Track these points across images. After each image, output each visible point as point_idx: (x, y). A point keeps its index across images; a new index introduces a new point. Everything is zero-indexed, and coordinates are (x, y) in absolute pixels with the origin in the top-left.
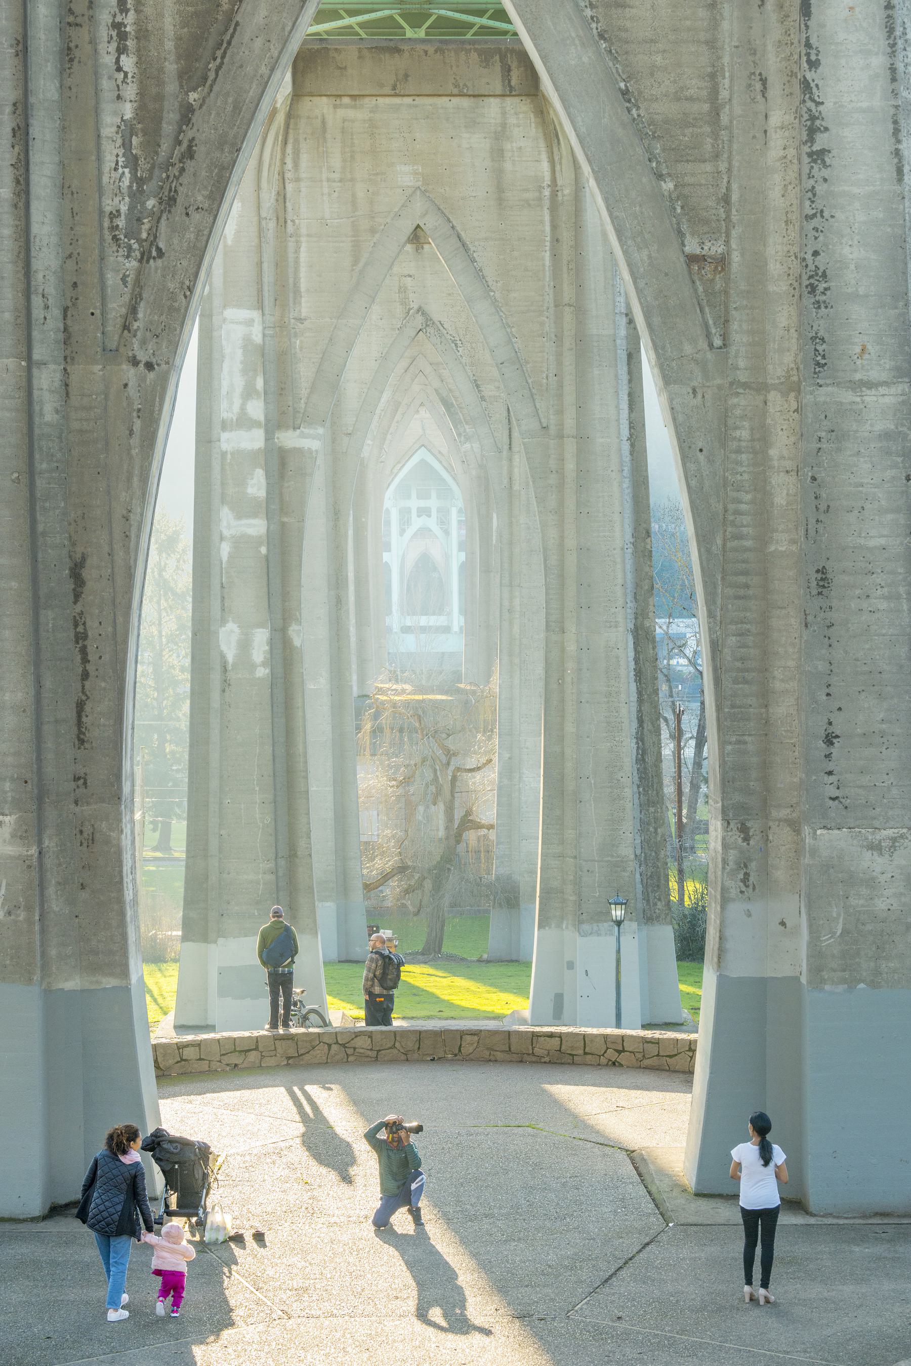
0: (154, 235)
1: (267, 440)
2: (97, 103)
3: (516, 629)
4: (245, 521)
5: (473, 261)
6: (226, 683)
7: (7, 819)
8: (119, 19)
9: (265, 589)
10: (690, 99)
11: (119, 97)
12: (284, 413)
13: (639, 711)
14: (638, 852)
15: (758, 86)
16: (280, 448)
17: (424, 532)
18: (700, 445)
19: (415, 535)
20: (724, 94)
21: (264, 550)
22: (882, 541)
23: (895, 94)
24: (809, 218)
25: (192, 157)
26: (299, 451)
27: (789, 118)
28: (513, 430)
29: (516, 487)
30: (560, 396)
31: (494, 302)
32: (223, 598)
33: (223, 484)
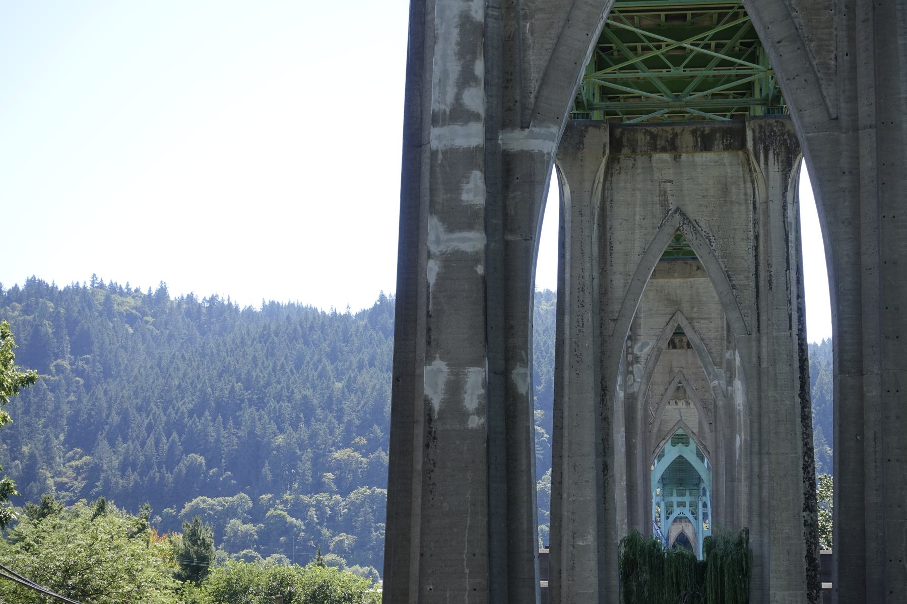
1: (487, 139)
3: (765, 493)
4: (457, 235)
9: (482, 318)
12: (510, 109)
16: (504, 151)
19: (675, 520)
21: (480, 269)
26: (529, 156)
28: (761, 315)
29: (764, 365)
30: (853, 79)
32: (429, 330)
33: (432, 190)
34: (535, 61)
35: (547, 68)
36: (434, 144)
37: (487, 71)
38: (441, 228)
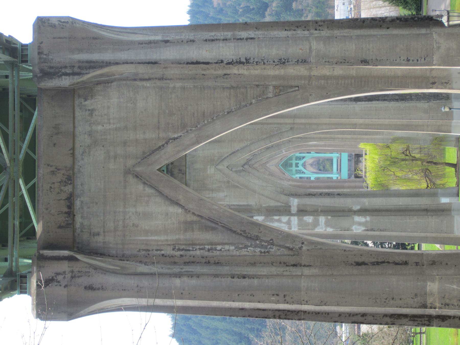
0: (266, 242)
2: (230, 256)
4: (320, 223)
5: (238, 150)
6: (372, 230)
7: (428, 284)
8: (207, 250)
10: (230, 95)
11: (228, 250)
13: (381, 100)
14: (426, 101)
15: (226, 76)
17: (304, 165)
18: (325, 94)
19: (305, 168)
20: (229, 86)
21: (329, 217)
22: (354, 45)
23: (230, 39)
24: (264, 64)
25: (245, 231)
27: (236, 68)
30: (281, 124)
31: (251, 144)
33: (309, 229)
34: (273, 203)
35: (275, 201)
36: (296, 229)
37: (276, 215)
38: (318, 227)
